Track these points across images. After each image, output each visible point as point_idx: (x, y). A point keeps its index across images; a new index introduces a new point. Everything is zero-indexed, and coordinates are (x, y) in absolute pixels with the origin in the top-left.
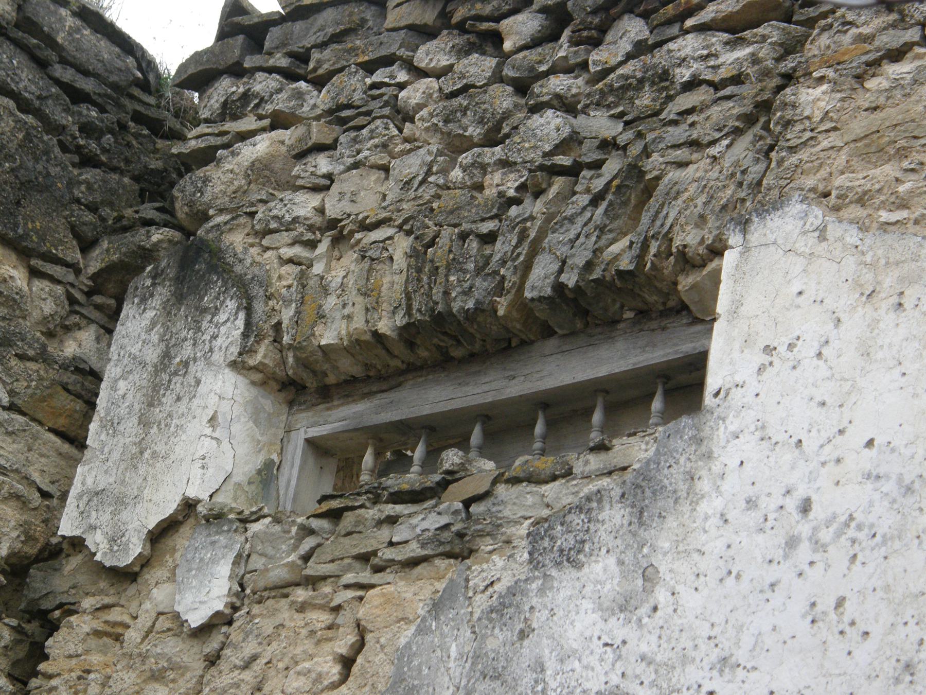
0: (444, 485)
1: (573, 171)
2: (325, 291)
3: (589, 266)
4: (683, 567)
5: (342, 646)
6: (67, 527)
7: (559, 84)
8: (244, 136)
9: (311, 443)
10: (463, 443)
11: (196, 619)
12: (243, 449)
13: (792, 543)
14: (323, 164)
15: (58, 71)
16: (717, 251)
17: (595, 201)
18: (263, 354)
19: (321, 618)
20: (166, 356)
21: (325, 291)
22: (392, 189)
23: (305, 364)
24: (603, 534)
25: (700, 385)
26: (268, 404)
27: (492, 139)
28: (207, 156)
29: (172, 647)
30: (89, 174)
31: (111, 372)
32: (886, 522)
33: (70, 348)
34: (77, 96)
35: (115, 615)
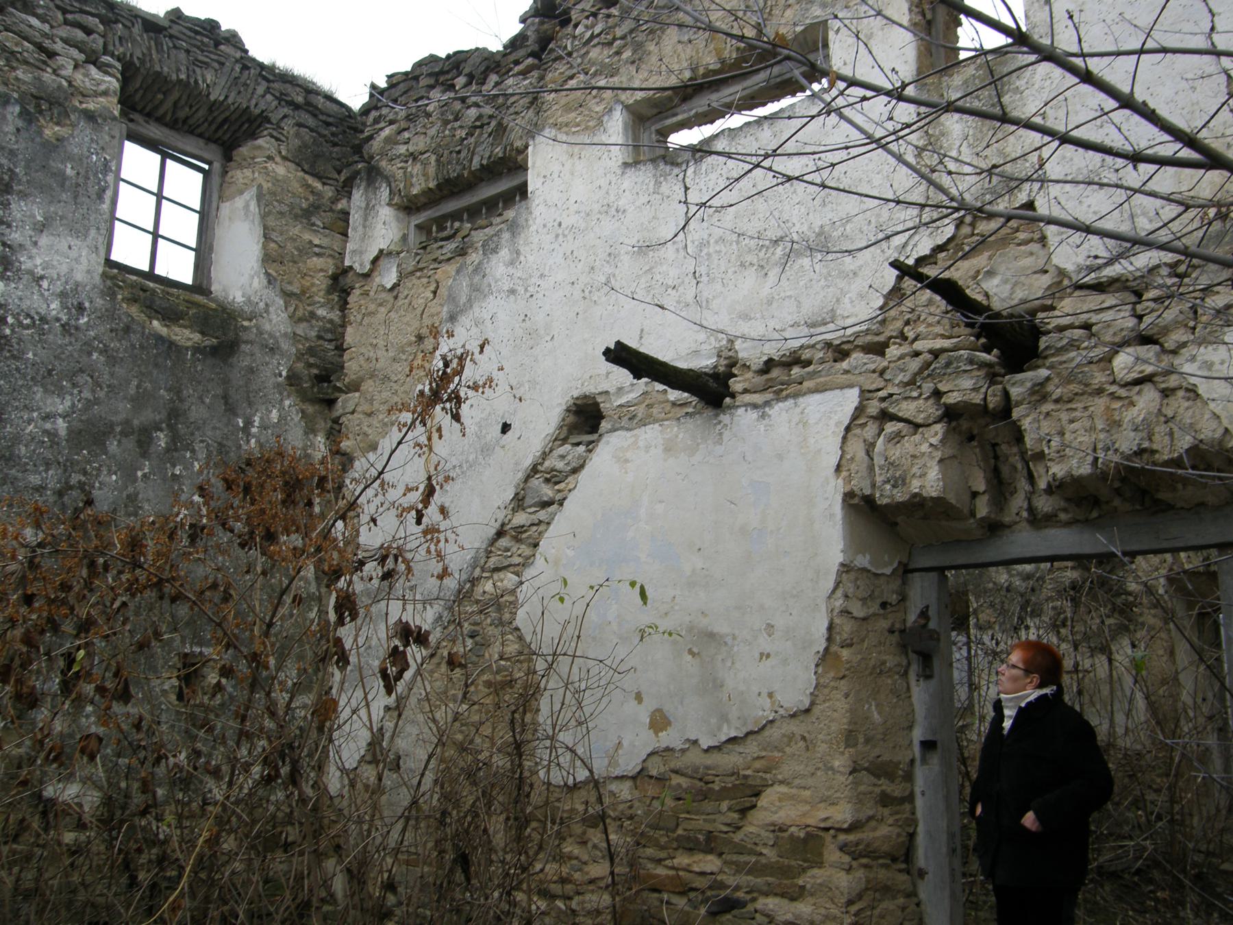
0: (455, 234)
1: (482, 127)
2: (412, 176)
3: (490, 157)
4: (527, 248)
5: (432, 288)
6: (347, 263)
7: (474, 99)
8: (381, 129)
9: (416, 226)
10: (461, 220)
11: (389, 286)
12: (395, 231)
13: (557, 236)
14: (406, 135)
15: (321, 117)
16: (526, 147)
17: (490, 135)
18: (396, 200)
19: (425, 280)
20: (368, 204)
21: (412, 176)
22: (428, 140)
23: (409, 201)
24: (503, 241)
25: (526, 191)
26: (401, 215)
27: (456, 119)
28: (371, 138)
29: (384, 295)
30: (336, 149)
31: (352, 212)
32: (583, 226)
33: (340, 206)
34: (328, 124)
35: (366, 288)
